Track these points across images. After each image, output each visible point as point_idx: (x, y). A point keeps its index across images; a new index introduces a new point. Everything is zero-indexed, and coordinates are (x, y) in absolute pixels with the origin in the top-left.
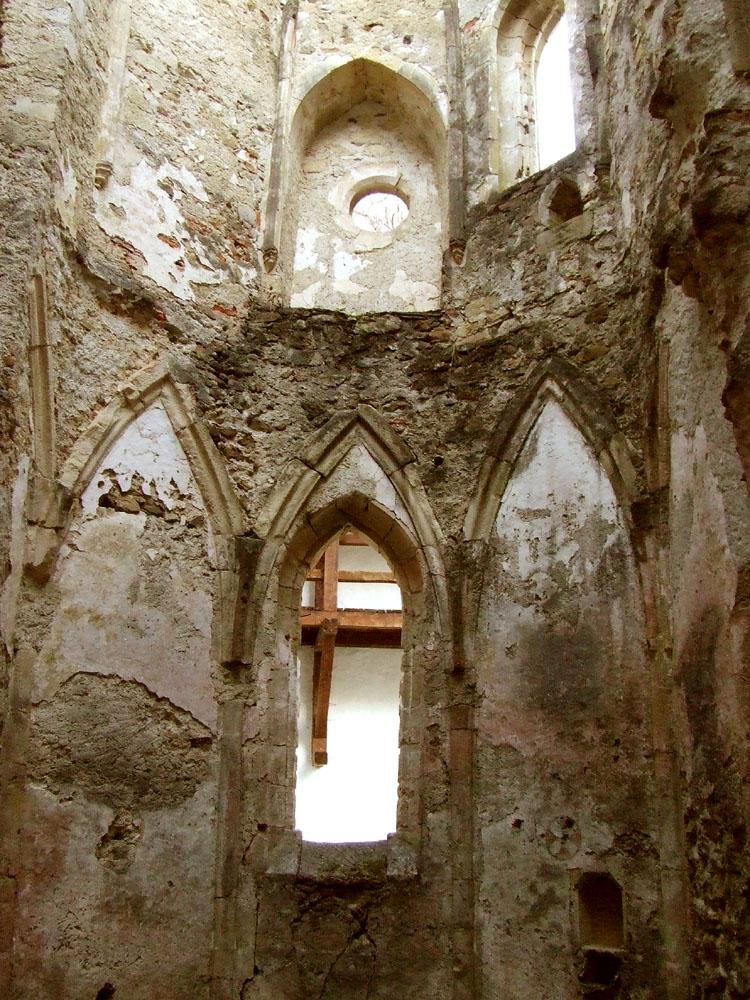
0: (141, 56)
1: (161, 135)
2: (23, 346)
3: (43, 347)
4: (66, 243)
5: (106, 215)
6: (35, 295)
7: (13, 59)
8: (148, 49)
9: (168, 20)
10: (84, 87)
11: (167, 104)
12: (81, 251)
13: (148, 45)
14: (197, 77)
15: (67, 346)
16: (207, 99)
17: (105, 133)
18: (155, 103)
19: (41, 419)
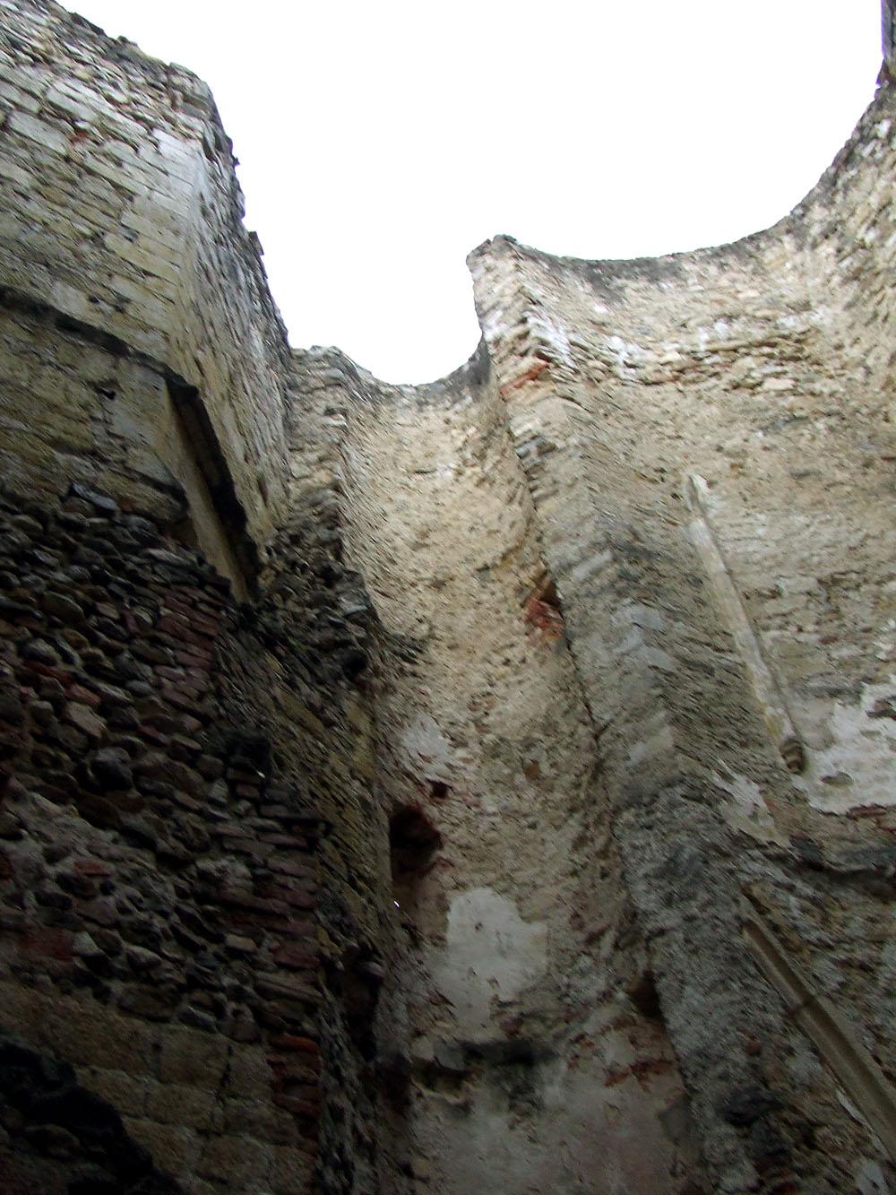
0: (771, 607)
1: (842, 664)
2: (774, 1019)
3: (810, 1002)
4: (780, 859)
5: (825, 795)
6: (758, 948)
7: (607, 717)
8: (776, 594)
9: (778, 551)
10: (707, 686)
11: (829, 629)
12: (809, 854)
13: (772, 592)
14: (848, 576)
15: (858, 979)
16: (874, 588)
17: (769, 711)
18: (815, 637)
19: (871, 1103)
